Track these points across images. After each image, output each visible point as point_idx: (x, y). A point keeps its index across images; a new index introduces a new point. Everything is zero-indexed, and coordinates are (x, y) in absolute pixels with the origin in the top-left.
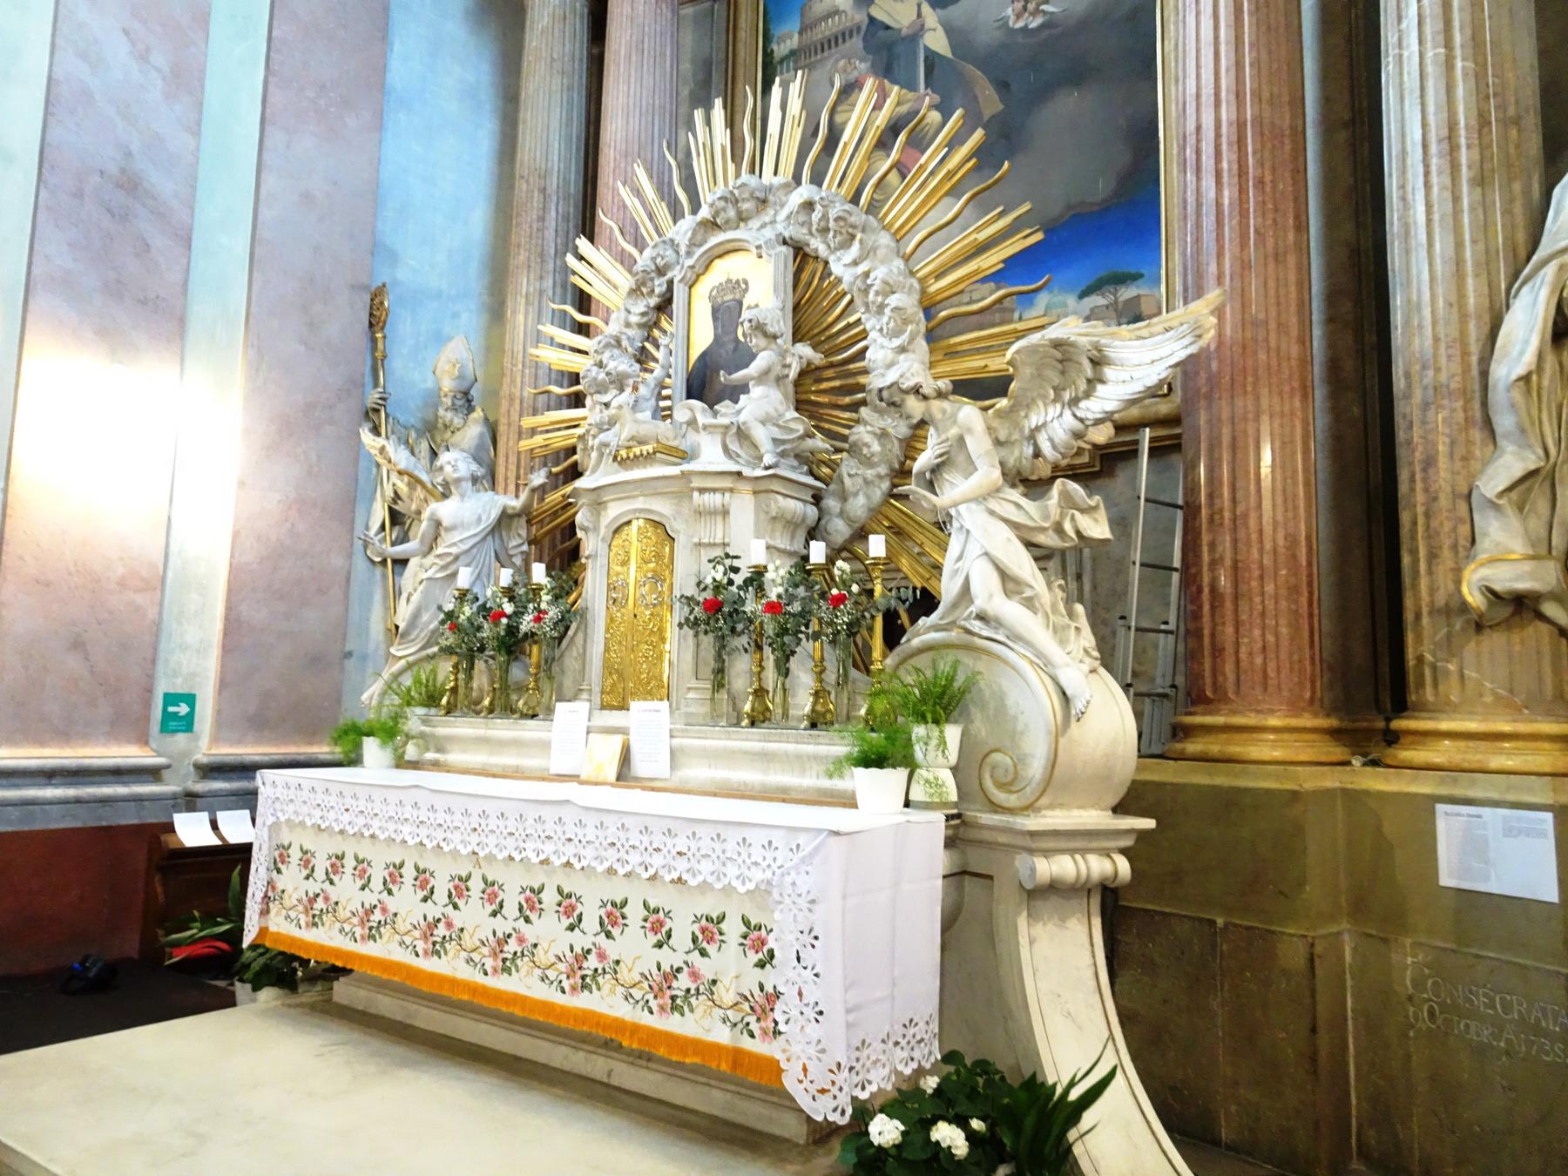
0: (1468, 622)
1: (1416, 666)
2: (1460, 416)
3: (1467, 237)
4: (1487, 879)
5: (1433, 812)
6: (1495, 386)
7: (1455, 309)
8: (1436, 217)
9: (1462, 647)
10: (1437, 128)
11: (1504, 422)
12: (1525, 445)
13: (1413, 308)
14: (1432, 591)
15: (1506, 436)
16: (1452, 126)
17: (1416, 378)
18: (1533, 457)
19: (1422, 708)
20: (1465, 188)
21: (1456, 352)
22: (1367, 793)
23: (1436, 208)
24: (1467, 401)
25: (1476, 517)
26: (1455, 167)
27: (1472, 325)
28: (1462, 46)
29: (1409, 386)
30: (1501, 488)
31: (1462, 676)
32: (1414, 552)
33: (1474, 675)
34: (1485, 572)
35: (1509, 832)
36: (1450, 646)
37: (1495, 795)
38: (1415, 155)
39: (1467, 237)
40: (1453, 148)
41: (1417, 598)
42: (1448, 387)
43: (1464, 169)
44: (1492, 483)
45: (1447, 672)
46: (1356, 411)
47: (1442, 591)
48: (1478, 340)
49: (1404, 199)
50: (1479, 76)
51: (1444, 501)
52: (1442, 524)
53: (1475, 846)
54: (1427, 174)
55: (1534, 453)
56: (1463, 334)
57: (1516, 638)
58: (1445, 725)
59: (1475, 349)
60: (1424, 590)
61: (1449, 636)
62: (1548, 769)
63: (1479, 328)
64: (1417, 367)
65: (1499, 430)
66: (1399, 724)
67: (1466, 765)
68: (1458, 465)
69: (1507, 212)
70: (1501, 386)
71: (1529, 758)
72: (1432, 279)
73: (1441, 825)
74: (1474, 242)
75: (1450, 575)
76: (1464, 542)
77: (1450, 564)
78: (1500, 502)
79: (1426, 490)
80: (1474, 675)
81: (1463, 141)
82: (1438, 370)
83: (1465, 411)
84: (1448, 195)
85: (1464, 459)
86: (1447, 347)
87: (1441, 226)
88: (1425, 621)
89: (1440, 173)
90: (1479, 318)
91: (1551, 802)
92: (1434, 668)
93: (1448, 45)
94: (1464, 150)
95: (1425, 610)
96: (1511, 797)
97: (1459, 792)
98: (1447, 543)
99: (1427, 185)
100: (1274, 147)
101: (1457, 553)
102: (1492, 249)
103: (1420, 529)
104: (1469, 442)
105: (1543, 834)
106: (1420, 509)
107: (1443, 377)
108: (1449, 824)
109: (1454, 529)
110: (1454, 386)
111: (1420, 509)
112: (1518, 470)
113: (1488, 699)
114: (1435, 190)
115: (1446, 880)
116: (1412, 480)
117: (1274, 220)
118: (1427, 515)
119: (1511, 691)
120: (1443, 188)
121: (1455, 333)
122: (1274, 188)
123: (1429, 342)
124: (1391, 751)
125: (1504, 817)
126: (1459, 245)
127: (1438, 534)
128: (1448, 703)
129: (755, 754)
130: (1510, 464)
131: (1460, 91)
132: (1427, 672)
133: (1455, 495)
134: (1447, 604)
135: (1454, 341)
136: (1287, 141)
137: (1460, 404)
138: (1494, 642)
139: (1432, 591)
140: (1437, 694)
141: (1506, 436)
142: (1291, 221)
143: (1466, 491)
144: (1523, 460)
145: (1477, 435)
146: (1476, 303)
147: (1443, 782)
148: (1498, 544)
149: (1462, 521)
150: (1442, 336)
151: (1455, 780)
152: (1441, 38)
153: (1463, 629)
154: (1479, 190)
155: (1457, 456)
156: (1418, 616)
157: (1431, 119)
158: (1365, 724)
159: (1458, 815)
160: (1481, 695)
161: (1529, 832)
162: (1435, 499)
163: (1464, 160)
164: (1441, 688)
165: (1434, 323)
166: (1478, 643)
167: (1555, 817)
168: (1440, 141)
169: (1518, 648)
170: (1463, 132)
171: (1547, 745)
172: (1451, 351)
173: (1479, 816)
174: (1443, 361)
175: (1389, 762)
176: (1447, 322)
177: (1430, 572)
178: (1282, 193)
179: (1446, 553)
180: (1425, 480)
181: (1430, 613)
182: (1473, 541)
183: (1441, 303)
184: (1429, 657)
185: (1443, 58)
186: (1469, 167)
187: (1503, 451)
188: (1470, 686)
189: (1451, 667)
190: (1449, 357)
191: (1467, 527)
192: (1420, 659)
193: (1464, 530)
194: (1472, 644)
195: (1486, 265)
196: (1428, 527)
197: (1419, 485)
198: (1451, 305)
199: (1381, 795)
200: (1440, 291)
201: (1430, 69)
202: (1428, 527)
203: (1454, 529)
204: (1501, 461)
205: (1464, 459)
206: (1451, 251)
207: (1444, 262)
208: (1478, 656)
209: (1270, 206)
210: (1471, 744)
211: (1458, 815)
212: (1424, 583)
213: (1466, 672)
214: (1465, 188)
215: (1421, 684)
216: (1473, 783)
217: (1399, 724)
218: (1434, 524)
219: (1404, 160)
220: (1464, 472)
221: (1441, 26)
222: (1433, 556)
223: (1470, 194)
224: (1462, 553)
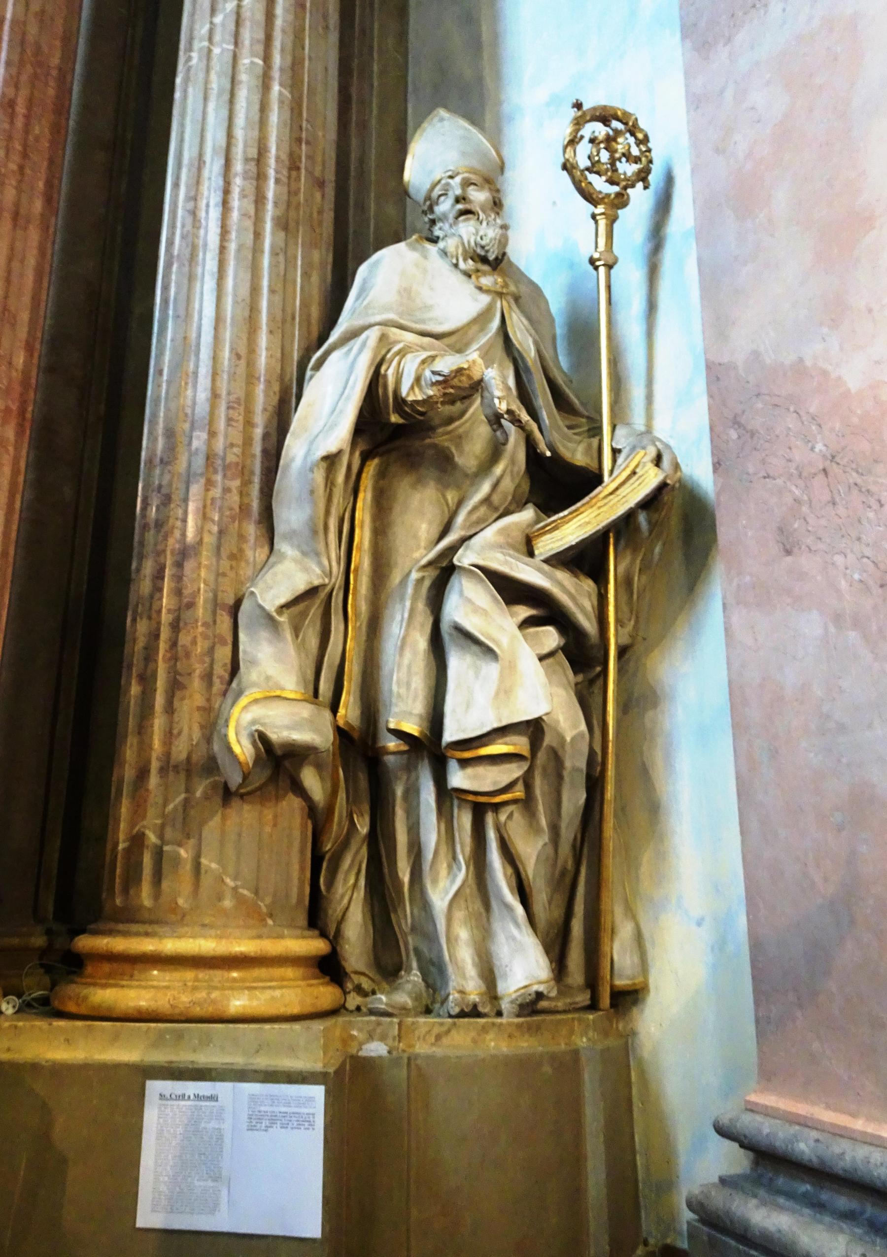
0: (214, 786)
1: (128, 851)
2: (234, 499)
3: (265, 283)
4: (214, 1208)
5: (141, 1095)
6: (288, 466)
7: (243, 362)
8: (232, 247)
9: (202, 823)
10: (246, 146)
11: (291, 515)
12: (310, 552)
13: (186, 348)
14: (170, 736)
15: (290, 536)
16: (262, 150)
17: (182, 439)
18: (318, 571)
19: (128, 918)
20: (268, 226)
21: (239, 416)
22: (35, 1067)
23: (233, 235)
24: (246, 483)
25: (242, 636)
26: (260, 200)
27: (260, 389)
28: (281, 70)
29: (171, 448)
30: (283, 600)
31: (197, 866)
32: (147, 680)
33: (214, 866)
34: (256, 712)
35: (258, 1121)
36: (187, 824)
37: (238, 1060)
38: (213, 168)
39: (265, 283)
40: (260, 177)
41: (144, 747)
42: (224, 459)
43: (270, 206)
44: (272, 592)
45: (177, 861)
46: (68, 492)
47: (184, 737)
48: (265, 410)
49: (194, 213)
50: (295, 108)
51: (201, 611)
52: (194, 642)
53: (203, 1153)
54: (226, 192)
55: (320, 564)
56: (249, 397)
57: (269, 814)
58: (170, 945)
59: (260, 420)
60: (161, 732)
61: (186, 803)
62: (296, 1010)
63: (266, 395)
64: (187, 426)
65: (280, 527)
66: (86, 943)
67: (197, 1011)
68: (225, 564)
69: (306, 275)
70: (297, 464)
71: (277, 993)
72: (219, 319)
73: (151, 1116)
74: (272, 291)
75: (197, 717)
76: (221, 671)
77: (199, 700)
78: (283, 619)
79: (178, 592)
80: (214, 866)
81: (271, 173)
82: (212, 434)
83: (241, 494)
84: (249, 224)
85: (233, 557)
86: (228, 408)
87: (237, 258)
88: (154, 780)
89: (243, 196)
90: (268, 382)
91: (318, 1067)
92: (159, 854)
93: (267, 58)
94: (271, 183)
95: (155, 765)
96: (262, 1062)
97: (185, 1057)
98: (199, 669)
99: (225, 204)
100: (35, 76)
101: (210, 684)
102: (289, 311)
103: (163, 646)
104: (242, 537)
105: (306, 1122)
106: (166, 618)
107: (220, 444)
108: (165, 1116)
109: (211, 651)
110: (231, 458)
111: (166, 618)
112: (301, 585)
113: (228, 903)
114: (235, 215)
115: (148, 1217)
116: (159, 575)
117: (21, 168)
118: (176, 626)
119: (256, 892)
120: (244, 215)
121: (240, 393)
122: (27, 129)
123: (203, 395)
124: (72, 989)
125: (253, 1098)
126: (255, 290)
127: (188, 655)
128: (174, 908)
129: (135, 812)
130: (287, 576)
131: (274, 118)
132: (147, 860)
133: (215, 604)
134: (189, 759)
135: (238, 401)
136: (52, 83)
137: (236, 484)
138: (245, 816)
139: (170, 736)
140: (157, 894)
141: (290, 536)
142: (41, 184)
143: (231, 601)
144: (306, 570)
145: (251, 530)
146: (267, 364)
147: (158, 1042)
148: (268, 678)
149: (223, 643)
150: (224, 393)
151: (179, 1036)
152: (260, 48)
153: (206, 797)
154: (282, 234)
155: (224, 553)
156: (143, 774)
157: (239, 134)
158: (16, 941)
159: (182, 1097)
160: (220, 899)
161: (287, 1121)
162: (191, 605)
163: (270, 195)
164: (165, 884)
165: (215, 375)
166: (224, 818)
167: (327, 1093)
168: (247, 160)
169: (268, 829)
170: (272, 162)
171: (289, 972)
172: (233, 414)
173: (213, 1098)
174: (221, 425)
175: (72, 1008)
176: (232, 376)
177: (170, 709)
178: (37, 139)
179: (196, 683)
180: (178, 578)
181: (163, 771)
182: (235, 668)
183: (226, 353)
184: (152, 838)
185: (259, 71)
186: (276, 204)
187: (282, 557)
188: (206, 881)
189: (183, 852)
190: (229, 420)
191: (228, 650)
192: (138, 840)
193: (224, 653)
194: (217, 818)
195: (281, 324)
196: (174, 644)
197: (167, 585)
198: (239, 357)
199: (60, 1073)
200: (227, 335)
201: (243, 77)
202: (174, 644)
203: (211, 651)
204: (279, 568)
205: (233, 557)
206: (245, 291)
207: (235, 302)
208: (223, 833)
209: (18, 147)
210: (203, 974)
211: (182, 1097)
212: (158, 723)
213: (204, 861)
214: (268, 226)
215: (132, 878)
216: (206, 1041)
217: (86, 943)
218: (184, 639)
219: (200, 169)
220: (232, 574)
221: (261, 35)
222: (176, 686)
223: (273, 234)
224: (218, 686)
